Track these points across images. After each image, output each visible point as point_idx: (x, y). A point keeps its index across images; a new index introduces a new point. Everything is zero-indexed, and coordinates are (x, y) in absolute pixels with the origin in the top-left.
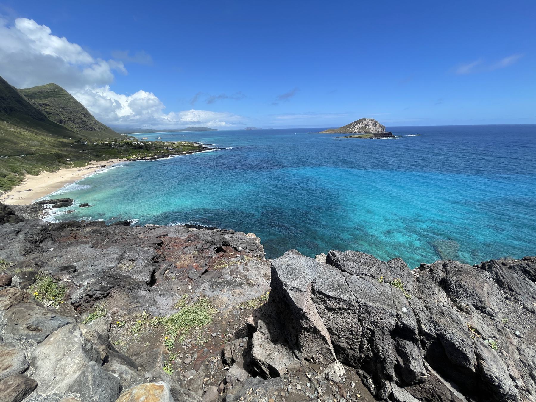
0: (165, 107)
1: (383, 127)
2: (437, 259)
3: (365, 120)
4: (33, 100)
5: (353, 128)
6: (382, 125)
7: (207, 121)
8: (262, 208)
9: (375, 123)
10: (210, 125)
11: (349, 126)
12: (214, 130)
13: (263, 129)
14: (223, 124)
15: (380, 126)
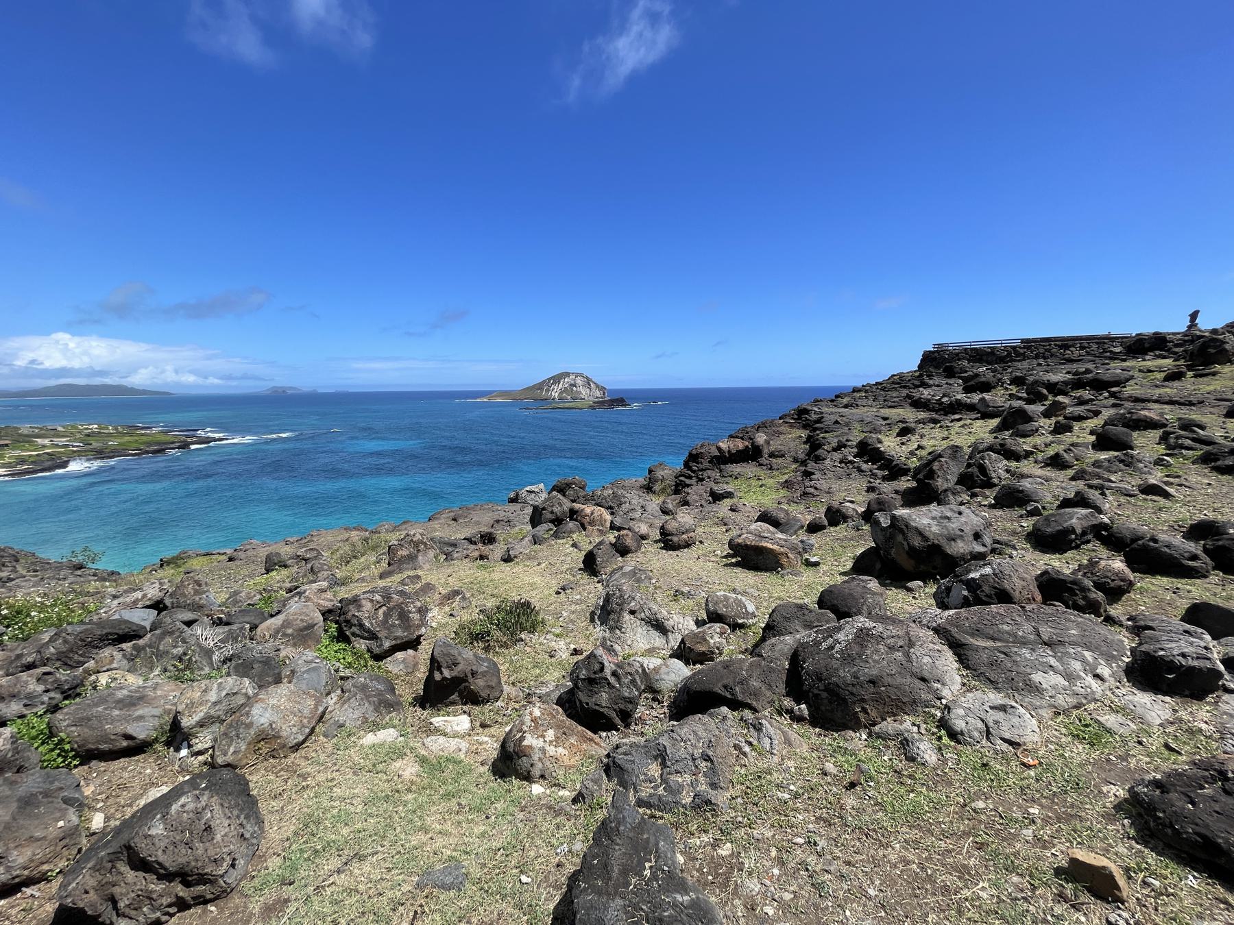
0: (364, 40)
1: (602, 389)
2: (957, 722)
3: (567, 374)
4: (1199, 453)
5: (548, 390)
6: (601, 384)
7: (134, 369)
8: (437, 731)
9: (588, 382)
10: (140, 379)
11: (540, 386)
12: (144, 392)
13: (320, 391)
14: (191, 379)
15: (597, 386)
